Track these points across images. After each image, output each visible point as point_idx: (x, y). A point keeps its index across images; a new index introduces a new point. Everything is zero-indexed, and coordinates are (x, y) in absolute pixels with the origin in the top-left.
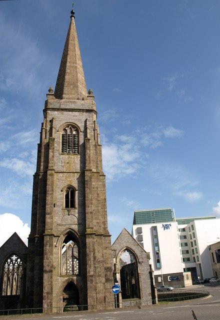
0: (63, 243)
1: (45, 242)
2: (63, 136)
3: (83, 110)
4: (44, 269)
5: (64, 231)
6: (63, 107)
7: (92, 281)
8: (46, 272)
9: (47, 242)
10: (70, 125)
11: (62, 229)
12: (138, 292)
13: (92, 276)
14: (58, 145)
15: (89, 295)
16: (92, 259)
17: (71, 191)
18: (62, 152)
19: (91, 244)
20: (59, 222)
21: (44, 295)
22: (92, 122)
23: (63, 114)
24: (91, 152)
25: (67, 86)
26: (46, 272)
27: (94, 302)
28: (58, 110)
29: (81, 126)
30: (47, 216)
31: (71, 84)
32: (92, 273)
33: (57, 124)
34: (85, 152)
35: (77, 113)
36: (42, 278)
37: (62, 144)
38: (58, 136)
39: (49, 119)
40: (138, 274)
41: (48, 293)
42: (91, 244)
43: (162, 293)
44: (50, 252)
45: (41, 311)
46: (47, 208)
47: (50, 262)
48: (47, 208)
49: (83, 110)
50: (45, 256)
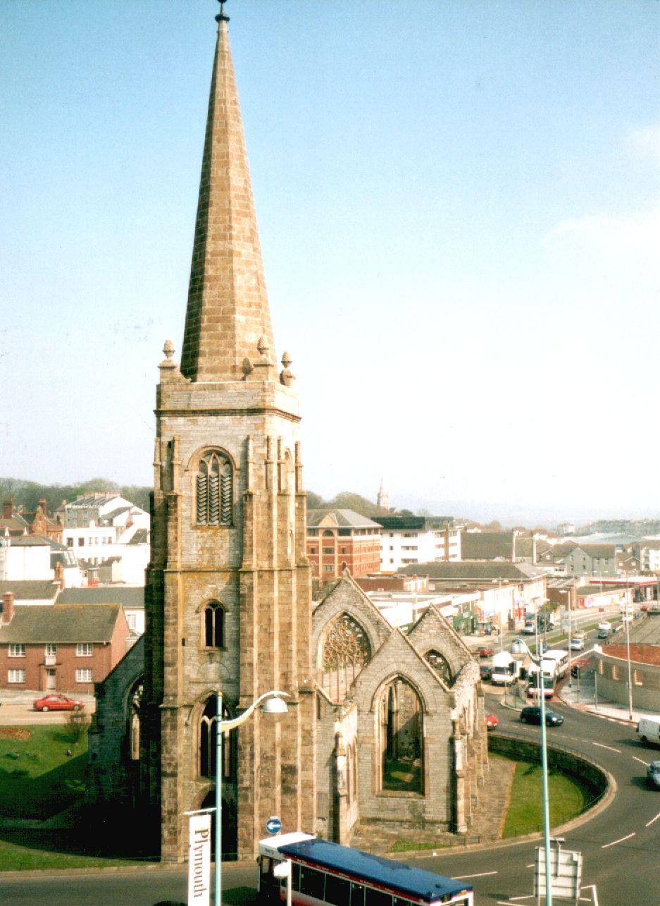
0: (204, 714)
1: (163, 720)
2: (198, 481)
3: (241, 412)
4: (163, 769)
5: (202, 695)
6: (197, 404)
7: (246, 798)
8: (166, 775)
9: (167, 720)
10: (214, 451)
11: (197, 690)
12: (150, 858)
13: (246, 789)
14: (186, 509)
15: (240, 821)
16: (248, 757)
17: (215, 614)
18: (198, 520)
19: (247, 729)
20: (194, 676)
21: (164, 814)
22: (260, 443)
23: (194, 423)
24: (255, 525)
25: (208, 329)
26: (166, 775)
27: (250, 834)
28: (183, 413)
29: (235, 451)
30: (168, 670)
31: (218, 321)
32: (246, 783)
33: (186, 454)
34: (243, 526)
35: (227, 420)
36: (159, 783)
37: (198, 501)
38: (185, 487)
39: (166, 439)
40: (423, 738)
41: (170, 812)
42: (247, 729)
43: (156, 857)
44: (171, 740)
45: (88, 526)
46: (168, 653)
47: (172, 759)
48: (168, 653)
49: (241, 412)
50: (164, 748)
